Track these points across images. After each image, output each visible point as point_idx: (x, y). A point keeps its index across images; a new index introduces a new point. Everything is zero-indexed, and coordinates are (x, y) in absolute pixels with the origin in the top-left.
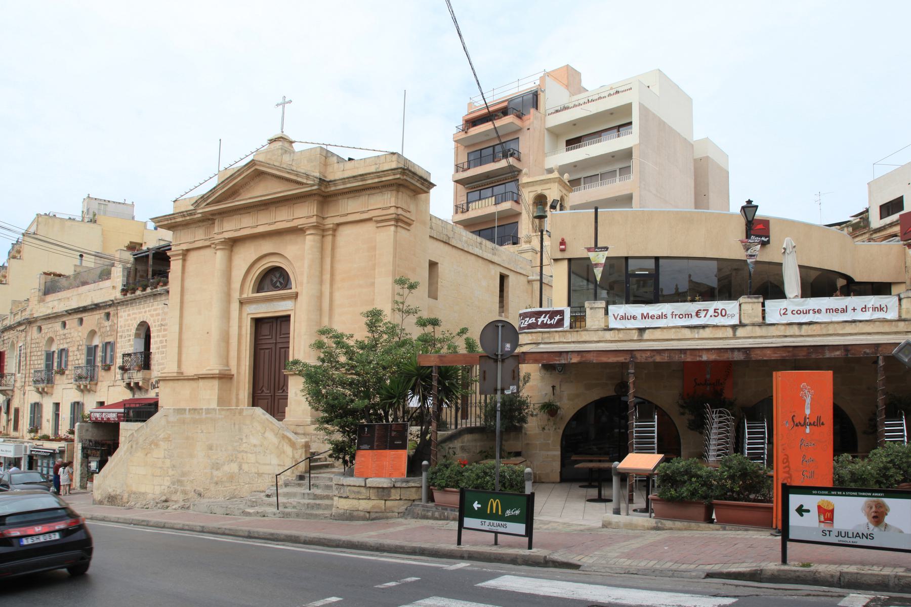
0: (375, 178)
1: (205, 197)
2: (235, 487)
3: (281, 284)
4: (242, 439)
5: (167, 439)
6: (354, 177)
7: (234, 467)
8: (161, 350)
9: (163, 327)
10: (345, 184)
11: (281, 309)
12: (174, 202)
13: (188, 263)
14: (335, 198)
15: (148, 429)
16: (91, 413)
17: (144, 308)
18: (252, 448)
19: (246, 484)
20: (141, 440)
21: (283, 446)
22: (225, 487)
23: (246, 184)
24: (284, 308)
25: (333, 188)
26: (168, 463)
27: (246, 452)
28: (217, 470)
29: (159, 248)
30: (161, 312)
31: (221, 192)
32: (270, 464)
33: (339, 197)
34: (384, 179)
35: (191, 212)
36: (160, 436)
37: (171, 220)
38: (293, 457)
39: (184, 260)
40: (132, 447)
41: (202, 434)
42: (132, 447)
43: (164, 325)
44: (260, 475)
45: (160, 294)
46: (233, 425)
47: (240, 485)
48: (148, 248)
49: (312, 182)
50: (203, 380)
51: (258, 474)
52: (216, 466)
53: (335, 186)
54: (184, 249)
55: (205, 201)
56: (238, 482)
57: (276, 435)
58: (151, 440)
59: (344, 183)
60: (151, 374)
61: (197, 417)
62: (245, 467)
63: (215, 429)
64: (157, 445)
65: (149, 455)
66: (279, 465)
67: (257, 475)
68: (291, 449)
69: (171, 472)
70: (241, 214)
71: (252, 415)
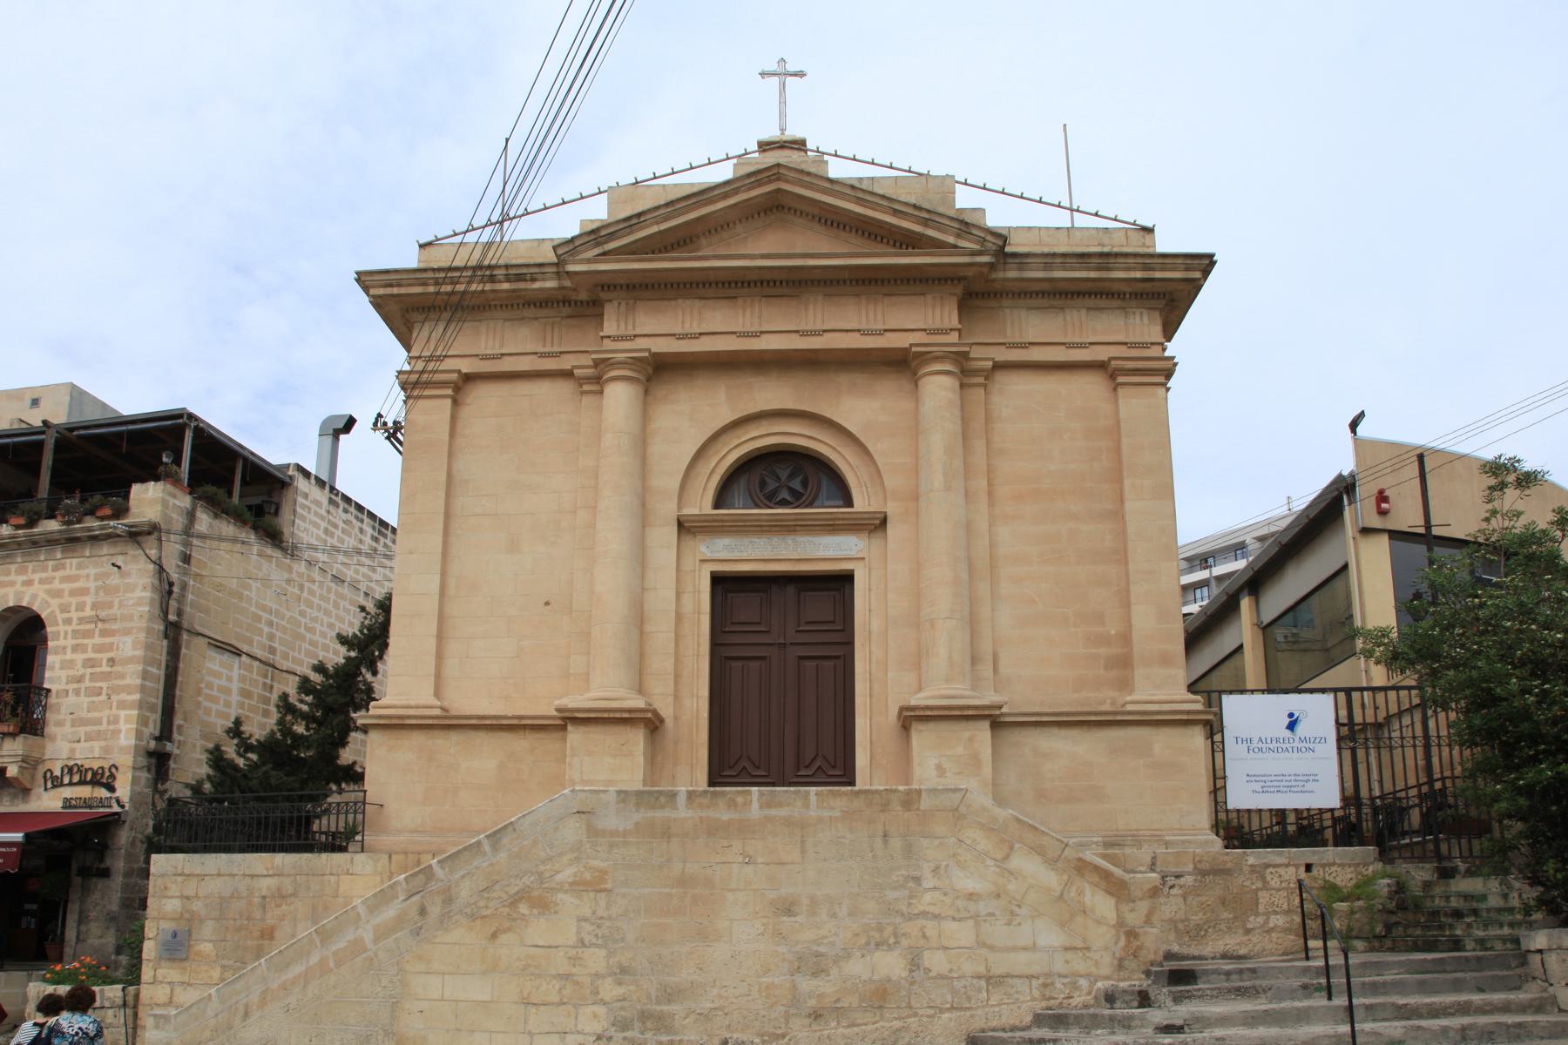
0: (1134, 269)
1: (603, 233)
2: (897, 1024)
3: (792, 491)
5: (594, 885)
6: (1082, 255)
7: (891, 964)
8: (87, 683)
9: (100, 625)
11: (821, 554)
12: (422, 246)
13: (465, 412)
14: (993, 303)
15: (503, 856)
17: (22, 571)
18: (960, 903)
19: (942, 1011)
20: (465, 892)
21: (1080, 893)
22: (853, 1025)
23: (727, 225)
24: (830, 554)
25: (1012, 274)
26: (596, 959)
27: (936, 917)
28: (815, 974)
29: (71, 430)
30: (92, 585)
31: (655, 229)
32: (1034, 948)
33: (1006, 302)
34: (1158, 275)
35: (524, 271)
36: (559, 877)
38: (1120, 923)
39: (455, 402)
40: (423, 911)
41: (749, 869)
42: (423, 911)
43: (103, 621)
44: (993, 980)
45: (94, 538)
46: (879, 842)
47: (916, 1015)
48: (45, 422)
50: (582, 729)
51: (988, 979)
52: (818, 967)
53: (1020, 269)
54: (464, 371)
55: (598, 244)
56: (910, 1007)
57: (1052, 862)
58: (513, 890)
59: (1048, 267)
60: (43, 747)
61: (725, 817)
62: (936, 962)
63: (803, 852)
64: (543, 905)
65: (503, 938)
66: (1066, 949)
67: (983, 983)
68: (1112, 902)
69: (609, 990)
70: (702, 298)
71: (957, 809)
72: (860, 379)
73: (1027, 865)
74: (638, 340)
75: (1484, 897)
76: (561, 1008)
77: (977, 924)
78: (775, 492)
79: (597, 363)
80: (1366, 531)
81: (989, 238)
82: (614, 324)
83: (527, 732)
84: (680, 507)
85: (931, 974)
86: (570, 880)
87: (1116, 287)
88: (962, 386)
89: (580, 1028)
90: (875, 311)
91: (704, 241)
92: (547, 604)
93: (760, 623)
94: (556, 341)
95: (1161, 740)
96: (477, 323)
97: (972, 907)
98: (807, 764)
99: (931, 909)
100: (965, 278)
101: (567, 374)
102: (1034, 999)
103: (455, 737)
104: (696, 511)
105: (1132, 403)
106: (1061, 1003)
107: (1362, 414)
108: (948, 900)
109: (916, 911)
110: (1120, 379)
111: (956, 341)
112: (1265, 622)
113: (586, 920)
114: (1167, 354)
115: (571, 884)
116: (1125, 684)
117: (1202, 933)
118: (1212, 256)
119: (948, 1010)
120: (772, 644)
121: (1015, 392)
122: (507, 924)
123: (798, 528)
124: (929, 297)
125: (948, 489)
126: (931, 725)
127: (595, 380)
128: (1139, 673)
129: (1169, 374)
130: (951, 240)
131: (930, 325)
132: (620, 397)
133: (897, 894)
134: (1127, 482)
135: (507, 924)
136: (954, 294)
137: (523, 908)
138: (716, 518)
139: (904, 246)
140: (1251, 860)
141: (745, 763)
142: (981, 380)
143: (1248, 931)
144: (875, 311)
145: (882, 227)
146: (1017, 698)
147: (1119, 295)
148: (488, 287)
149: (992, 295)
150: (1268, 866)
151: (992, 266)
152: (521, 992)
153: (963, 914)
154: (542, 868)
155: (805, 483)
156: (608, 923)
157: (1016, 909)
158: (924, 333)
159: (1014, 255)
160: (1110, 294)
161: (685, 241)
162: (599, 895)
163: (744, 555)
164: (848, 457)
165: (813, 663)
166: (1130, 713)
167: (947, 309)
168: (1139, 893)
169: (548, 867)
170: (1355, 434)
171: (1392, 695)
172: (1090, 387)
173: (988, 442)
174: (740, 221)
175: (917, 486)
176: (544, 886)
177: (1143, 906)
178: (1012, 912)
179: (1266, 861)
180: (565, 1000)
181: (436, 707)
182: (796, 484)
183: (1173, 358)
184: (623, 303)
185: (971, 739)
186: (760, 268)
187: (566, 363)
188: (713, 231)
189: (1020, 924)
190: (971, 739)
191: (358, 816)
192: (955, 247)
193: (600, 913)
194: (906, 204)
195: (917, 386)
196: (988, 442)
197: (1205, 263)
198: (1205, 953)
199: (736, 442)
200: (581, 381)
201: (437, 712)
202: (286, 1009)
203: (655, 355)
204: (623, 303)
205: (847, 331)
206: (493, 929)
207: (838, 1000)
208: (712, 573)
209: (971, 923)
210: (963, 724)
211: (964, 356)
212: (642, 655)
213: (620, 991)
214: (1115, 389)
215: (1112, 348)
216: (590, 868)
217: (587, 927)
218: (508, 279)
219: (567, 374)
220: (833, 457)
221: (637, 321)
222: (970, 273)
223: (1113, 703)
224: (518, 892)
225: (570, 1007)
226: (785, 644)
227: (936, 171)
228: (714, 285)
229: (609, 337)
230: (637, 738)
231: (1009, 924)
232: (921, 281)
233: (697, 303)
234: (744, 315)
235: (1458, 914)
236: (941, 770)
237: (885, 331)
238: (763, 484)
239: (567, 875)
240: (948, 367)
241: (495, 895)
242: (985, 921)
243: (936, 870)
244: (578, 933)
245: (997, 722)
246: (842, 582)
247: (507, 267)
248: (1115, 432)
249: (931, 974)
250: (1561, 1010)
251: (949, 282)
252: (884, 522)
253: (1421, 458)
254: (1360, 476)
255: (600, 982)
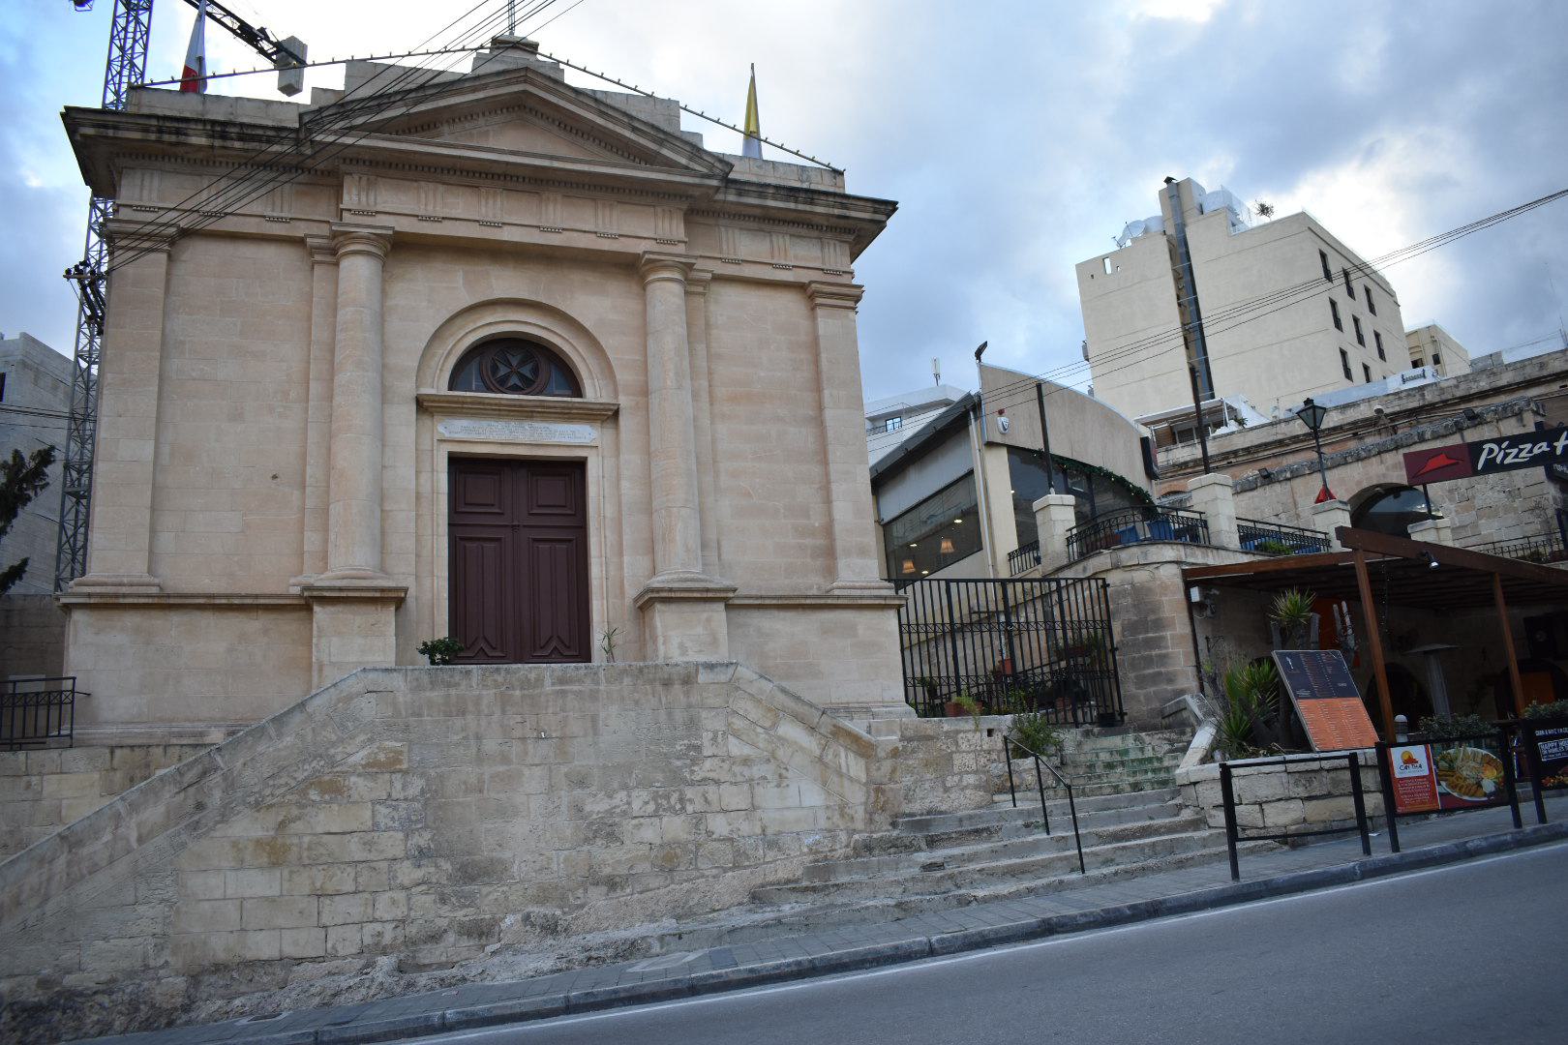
2: (686, 886)
3: (522, 377)
4: (698, 748)
7: (675, 827)
10: (765, 198)
11: (555, 440)
14: (711, 221)
16: (969, 696)
21: (836, 755)
25: (732, 198)
33: (722, 221)
34: (853, 214)
36: (352, 760)
37: (160, 131)
39: (170, 256)
47: (703, 876)
49: (705, 170)
59: (762, 195)
64: (334, 790)
68: (862, 762)
72: (592, 278)
73: (790, 730)
74: (379, 216)
75: (1126, 752)
76: (357, 896)
77: (751, 787)
78: (507, 377)
79: (335, 235)
80: (990, 445)
81: (717, 164)
82: (355, 198)
83: (260, 612)
84: (417, 387)
85: (714, 836)
86: (363, 763)
87: (816, 220)
88: (687, 293)
89: (378, 914)
90: (611, 217)
91: (446, 128)
92: (275, 477)
93: (493, 505)
94: (286, 208)
95: (864, 620)
96: (196, 178)
97: (747, 772)
98: (543, 643)
99: (712, 775)
100: (691, 196)
101: (298, 242)
102: (802, 854)
103: (176, 618)
104: (433, 391)
105: (828, 323)
106: (826, 856)
107: (985, 345)
108: (726, 766)
109: (698, 778)
110: (819, 301)
111: (683, 252)
112: (886, 520)
113: (380, 802)
114: (854, 282)
115: (364, 767)
116: (831, 571)
117: (911, 793)
118: (897, 203)
119: (731, 869)
120: (506, 526)
121: (729, 302)
122: (295, 812)
123: (535, 414)
124: (659, 210)
125: (680, 387)
126: (674, 607)
127: (332, 251)
128: (842, 563)
129: (857, 299)
130: (684, 161)
131: (660, 234)
132: (358, 271)
133: (679, 763)
134: (826, 393)
135: (295, 812)
136: (680, 209)
137: (314, 795)
138: (450, 399)
139: (637, 160)
140: (946, 727)
141: (483, 645)
142: (700, 289)
143: (946, 790)
144: (611, 217)
145: (620, 141)
146: (747, 584)
147: (818, 227)
148: (218, 143)
149: (711, 214)
150: (958, 732)
151: (718, 189)
152: (313, 883)
153: (740, 779)
154: (332, 751)
155: (536, 371)
156: (404, 805)
157: (784, 772)
158: (654, 242)
159: (735, 181)
160: (810, 225)
161: (429, 126)
162: (394, 776)
163: (482, 437)
164: (581, 351)
165: (547, 546)
166: (838, 597)
167: (675, 222)
168: (882, 754)
169: (340, 749)
170: (980, 361)
171: (1019, 585)
172: (789, 305)
173: (708, 347)
174: (484, 114)
175: (647, 382)
176: (335, 770)
177: (887, 766)
178: (780, 776)
179: (958, 728)
180: (361, 889)
181: (153, 585)
182: (526, 371)
183: (861, 287)
184: (365, 178)
185: (709, 620)
186: (507, 163)
187: (299, 230)
188: (457, 120)
189: (788, 785)
190: (709, 620)
191: (925, 639)
192: (687, 168)
193: (395, 795)
194: (645, 123)
195: (644, 289)
196: (708, 347)
197: (890, 207)
198: (914, 810)
199: (472, 326)
200: (313, 251)
201: (154, 590)
202: (22, 926)
203: (397, 233)
204: (365, 178)
205: (585, 232)
206: (280, 818)
207: (631, 868)
208: (449, 453)
209: (746, 787)
210: (701, 607)
211: (690, 266)
212: (383, 533)
213: (419, 874)
214: (813, 309)
215: (811, 272)
216: (385, 749)
217: (383, 810)
218: (241, 138)
219: (298, 242)
220: (566, 348)
221: (378, 198)
222: (697, 193)
223: (819, 589)
224: (306, 778)
225: (366, 895)
226: (519, 526)
227: (661, 94)
228: (458, 173)
229: (350, 210)
230: (388, 616)
231: (778, 786)
232: (653, 194)
233: (441, 188)
234: (487, 203)
235: (1110, 766)
236: (683, 649)
237: (620, 236)
238: (495, 369)
239: (360, 757)
240: (677, 275)
241: (282, 781)
242: (758, 784)
243: (714, 739)
244: (373, 816)
245: (729, 601)
246: (573, 470)
247: (242, 125)
248: (814, 345)
249: (714, 836)
250: (1210, 827)
251: (678, 198)
252: (616, 414)
253: (1039, 387)
254: (986, 396)
255: (398, 866)
